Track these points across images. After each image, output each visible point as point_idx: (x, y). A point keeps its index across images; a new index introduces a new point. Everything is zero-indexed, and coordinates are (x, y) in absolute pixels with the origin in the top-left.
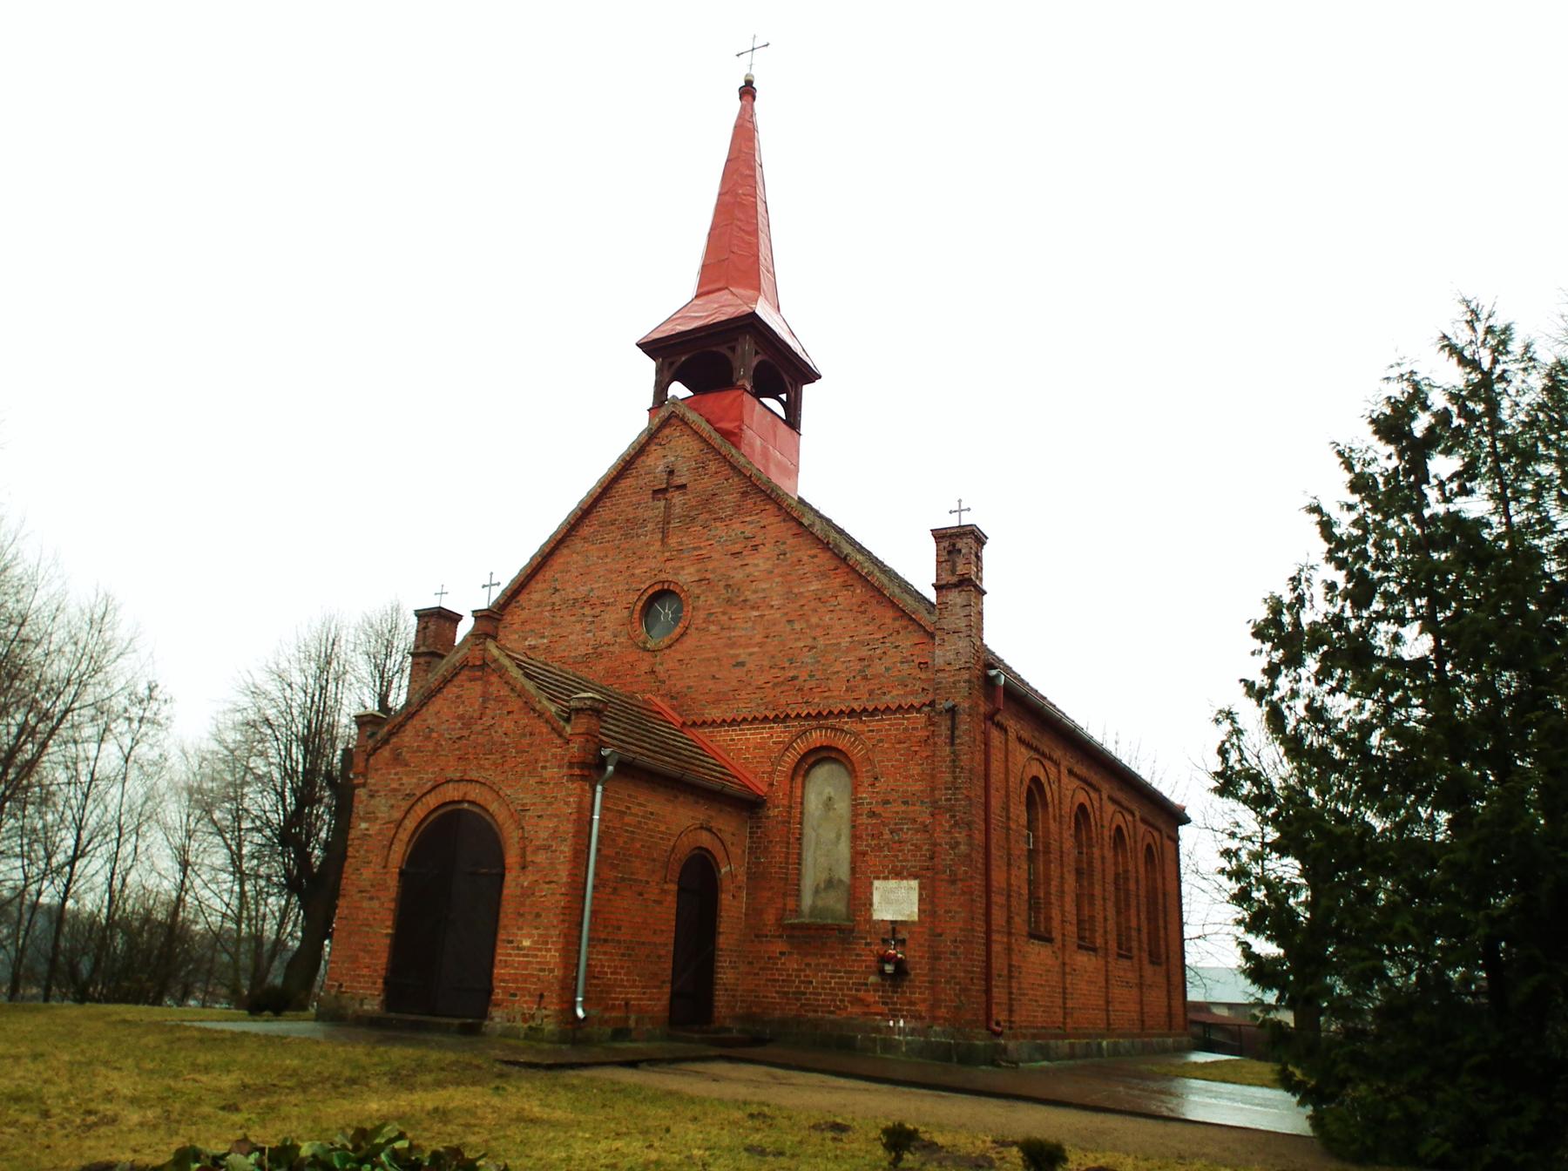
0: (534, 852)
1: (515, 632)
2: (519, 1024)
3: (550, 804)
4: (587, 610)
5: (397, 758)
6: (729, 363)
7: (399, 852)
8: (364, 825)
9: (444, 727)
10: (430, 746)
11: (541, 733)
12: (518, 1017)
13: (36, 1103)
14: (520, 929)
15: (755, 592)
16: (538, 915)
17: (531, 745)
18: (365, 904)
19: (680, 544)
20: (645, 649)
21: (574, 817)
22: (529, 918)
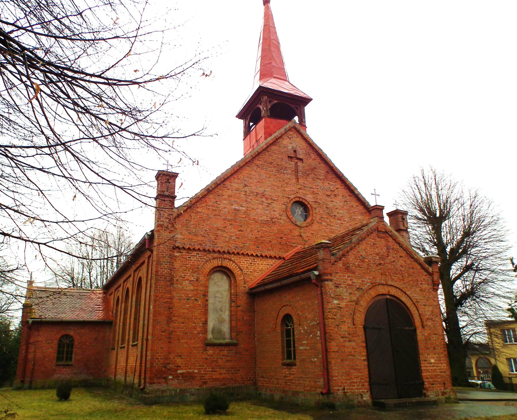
0: (426, 321)
1: (225, 199)
2: (441, 397)
4: (264, 200)
5: (347, 269)
6: (274, 109)
7: (360, 318)
8: (336, 302)
9: (370, 257)
10: (365, 265)
11: (416, 269)
12: (440, 394)
14: (428, 355)
15: (338, 213)
17: (414, 273)
18: (347, 344)
19: (304, 183)
20: (296, 225)
22: (432, 349)
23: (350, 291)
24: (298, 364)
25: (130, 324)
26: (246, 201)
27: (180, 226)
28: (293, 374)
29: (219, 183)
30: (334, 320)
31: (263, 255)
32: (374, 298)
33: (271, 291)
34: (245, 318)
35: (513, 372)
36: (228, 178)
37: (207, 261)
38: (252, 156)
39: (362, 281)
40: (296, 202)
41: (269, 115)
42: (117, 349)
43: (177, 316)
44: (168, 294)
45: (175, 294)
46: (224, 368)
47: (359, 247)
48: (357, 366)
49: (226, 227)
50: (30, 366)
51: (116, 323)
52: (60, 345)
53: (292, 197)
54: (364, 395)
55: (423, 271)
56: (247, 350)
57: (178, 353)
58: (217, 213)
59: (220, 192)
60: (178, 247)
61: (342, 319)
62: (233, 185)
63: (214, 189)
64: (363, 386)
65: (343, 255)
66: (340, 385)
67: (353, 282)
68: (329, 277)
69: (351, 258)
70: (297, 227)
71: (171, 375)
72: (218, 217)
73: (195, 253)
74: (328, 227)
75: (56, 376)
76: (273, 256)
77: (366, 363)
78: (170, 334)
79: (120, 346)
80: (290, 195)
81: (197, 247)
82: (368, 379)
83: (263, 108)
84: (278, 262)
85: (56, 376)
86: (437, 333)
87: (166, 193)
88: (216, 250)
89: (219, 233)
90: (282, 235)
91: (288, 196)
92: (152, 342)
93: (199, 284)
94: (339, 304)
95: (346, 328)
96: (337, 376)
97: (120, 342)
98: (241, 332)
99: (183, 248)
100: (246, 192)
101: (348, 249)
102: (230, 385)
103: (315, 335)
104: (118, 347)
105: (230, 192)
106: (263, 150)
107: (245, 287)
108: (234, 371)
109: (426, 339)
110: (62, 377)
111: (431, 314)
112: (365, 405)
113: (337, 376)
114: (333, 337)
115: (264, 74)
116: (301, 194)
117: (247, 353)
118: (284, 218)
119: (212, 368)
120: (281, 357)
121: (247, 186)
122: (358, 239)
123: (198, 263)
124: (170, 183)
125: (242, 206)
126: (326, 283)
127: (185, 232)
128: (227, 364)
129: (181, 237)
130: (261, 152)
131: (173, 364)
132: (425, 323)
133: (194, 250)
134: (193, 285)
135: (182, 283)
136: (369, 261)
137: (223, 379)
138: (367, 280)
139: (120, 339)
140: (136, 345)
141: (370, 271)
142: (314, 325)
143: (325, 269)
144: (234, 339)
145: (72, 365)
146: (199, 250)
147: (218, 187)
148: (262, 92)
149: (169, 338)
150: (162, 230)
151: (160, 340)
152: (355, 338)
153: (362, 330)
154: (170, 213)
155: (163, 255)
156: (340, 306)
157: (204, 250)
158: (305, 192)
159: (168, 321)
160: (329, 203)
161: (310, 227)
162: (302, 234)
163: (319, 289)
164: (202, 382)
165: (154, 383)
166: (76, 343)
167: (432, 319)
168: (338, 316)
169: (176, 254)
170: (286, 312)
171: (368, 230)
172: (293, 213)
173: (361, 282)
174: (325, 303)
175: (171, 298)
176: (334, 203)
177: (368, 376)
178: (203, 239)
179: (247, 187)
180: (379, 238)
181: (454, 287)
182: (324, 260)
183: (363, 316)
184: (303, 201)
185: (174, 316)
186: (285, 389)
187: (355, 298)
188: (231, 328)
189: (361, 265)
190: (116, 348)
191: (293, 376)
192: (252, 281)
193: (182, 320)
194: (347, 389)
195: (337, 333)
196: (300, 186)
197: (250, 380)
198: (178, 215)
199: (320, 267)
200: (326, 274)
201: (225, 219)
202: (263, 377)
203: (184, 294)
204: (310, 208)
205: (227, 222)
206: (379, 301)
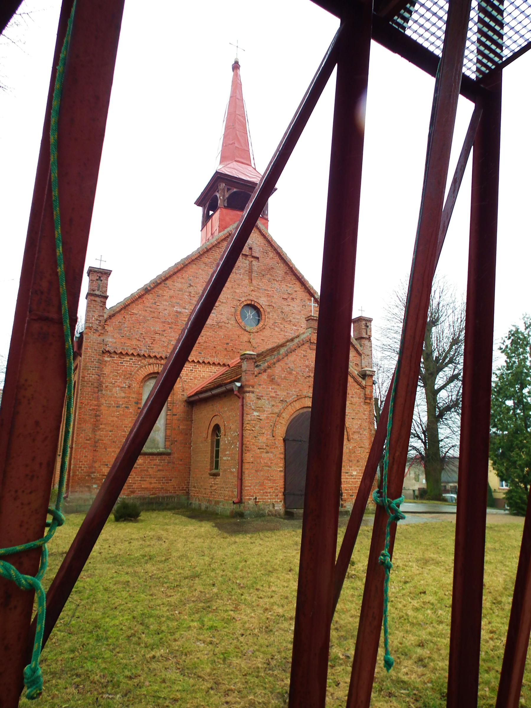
1: (166, 300)
3: (356, 414)
5: (272, 380)
7: (281, 431)
8: (256, 414)
9: (299, 369)
10: (292, 378)
13: (431, 562)
14: (351, 467)
15: (294, 318)
16: (358, 461)
18: (264, 455)
20: (245, 330)
21: (368, 420)
22: (355, 462)
23: (273, 403)
24: (221, 474)
25: (62, 431)
26: (190, 303)
27: (112, 329)
28: (217, 484)
29: (159, 282)
30: (252, 432)
31: (206, 361)
32: (298, 410)
33: (206, 400)
34: (181, 427)
35: (502, 486)
36: (170, 276)
37: (141, 367)
38: (199, 252)
39: (288, 393)
40: (248, 305)
41: (226, 205)
43: (105, 424)
44: (95, 401)
45: (103, 401)
46: (154, 478)
47: (288, 359)
48: (272, 477)
49: (164, 331)
53: (243, 299)
54: (276, 505)
55: (356, 384)
56: (181, 460)
57: (105, 462)
58: (155, 315)
59: (161, 292)
60: (109, 352)
61: (261, 431)
62: (176, 284)
63: (153, 288)
64: (277, 495)
65: (269, 367)
66: (252, 494)
67: (278, 395)
68: (251, 389)
69: (277, 370)
70: (246, 332)
71: (95, 483)
72: (157, 320)
73: (128, 358)
74: (282, 333)
76: (216, 363)
77: (282, 474)
78: (96, 442)
80: (241, 298)
81: (130, 352)
82: (283, 490)
83: (220, 197)
84: (223, 370)
86: (363, 446)
87: (97, 293)
88: (152, 355)
89: (157, 337)
90: (228, 341)
91: (238, 299)
92: (75, 450)
93: (131, 391)
94: (259, 416)
95: (264, 439)
96: (250, 486)
98: (176, 441)
99: (115, 352)
100: (190, 292)
101: (275, 360)
102: (161, 495)
103: (235, 446)
105: (172, 293)
106: (213, 246)
107: (183, 395)
108: (165, 480)
109: (350, 452)
111: (359, 427)
112: (276, 515)
113: (250, 486)
114: (249, 449)
115: (224, 158)
116: (253, 297)
117: (180, 463)
118: (233, 322)
119: (141, 478)
120: (209, 467)
121: (192, 286)
122: (287, 351)
123: (131, 369)
124: (102, 280)
125: (185, 309)
126: (247, 394)
127: (117, 335)
128: (159, 473)
129: (112, 341)
130: (211, 249)
131: (98, 472)
132: (351, 436)
133: (127, 354)
134: (124, 392)
135: (112, 389)
136: (297, 373)
137: (153, 488)
138: (294, 392)
141: (297, 384)
142: (235, 435)
143: (246, 381)
144: (168, 448)
146: (133, 354)
147: (159, 286)
148: (219, 178)
149: (95, 446)
150: (90, 332)
151: (85, 448)
152: (273, 450)
153: (282, 441)
154: (101, 314)
155: (91, 359)
156: (261, 418)
157: (139, 355)
158: (258, 294)
159: (93, 429)
160: (284, 307)
161: (261, 333)
162: (251, 340)
163: (241, 400)
164: (130, 491)
165: (76, 492)
167: (360, 432)
168: (257, 428)
169: (107, 359)
170: (216, 422)
171: (299, 341)
172: (243, 317)
173: (285, 394)
174: (245, 415)
175: (99, 406)
176: (291, 308)
177: (283, 486)
178: (138, 343)
179: (191, 287)
180: (311, 349)
181: (438, 396)
182: (247, 372)
183: (285, 429)
184: (256, 304)
185: (102, 424)
186: (211, 499)
187: (277, 410)
188: (167, 438)
189: (288, 377)
191: (216, 486)
192: (192, 389)
193: (110, 428)
194: (259, 499)
195: (253, 445)
196: (252, 288)
197: (183, 490)
198: (110, 316)
199: (243, 379)
200: (249, 386)
201: (164, 322)
202: (194, 487)
203: (113, 401)
204: (262, 312)
205: (167, 326)
206: (302, 414)
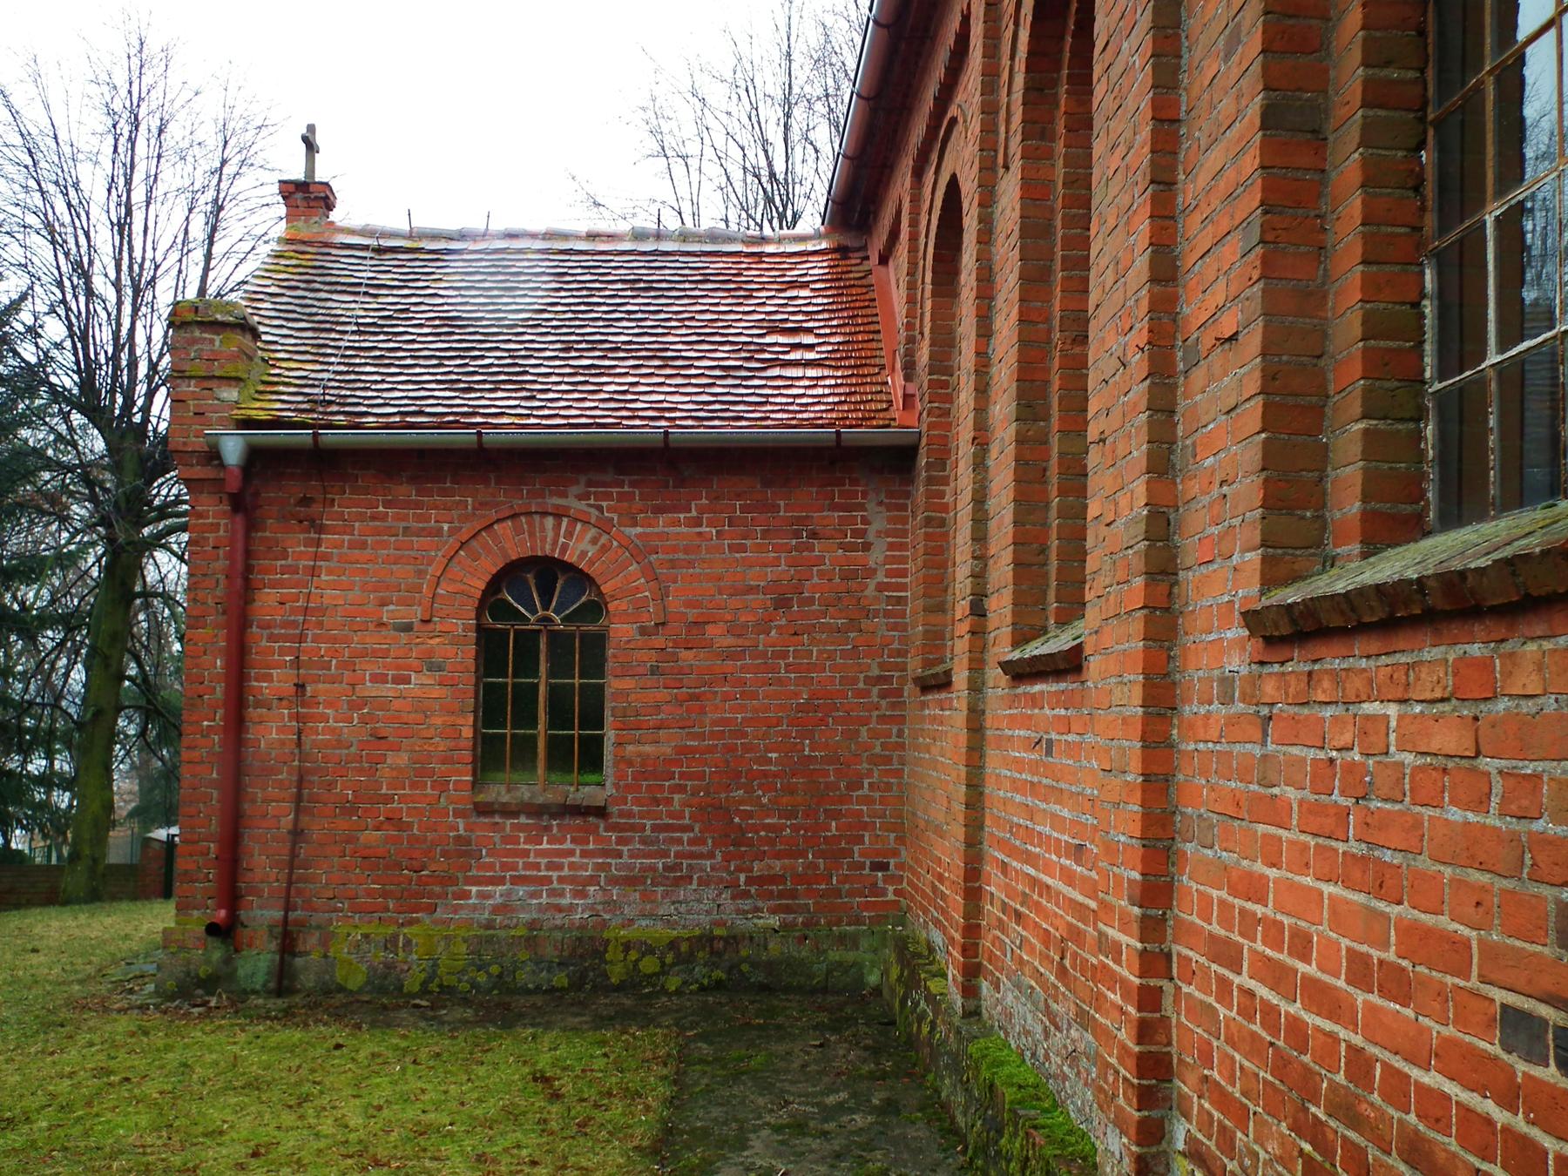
42: (976, 687)
50: (271, 808)
51: (943, 457)
52: (500, 647)
75: (480, 901)
79: (1002, 649)
85: (480, 901)
97: (1001, 607)
104: (977, 665)
110: (530, 904)
139: (1002, 570)
140: (1070, 664)
145: (601, 812)
166: (621, 631)
190: (960, 678)
